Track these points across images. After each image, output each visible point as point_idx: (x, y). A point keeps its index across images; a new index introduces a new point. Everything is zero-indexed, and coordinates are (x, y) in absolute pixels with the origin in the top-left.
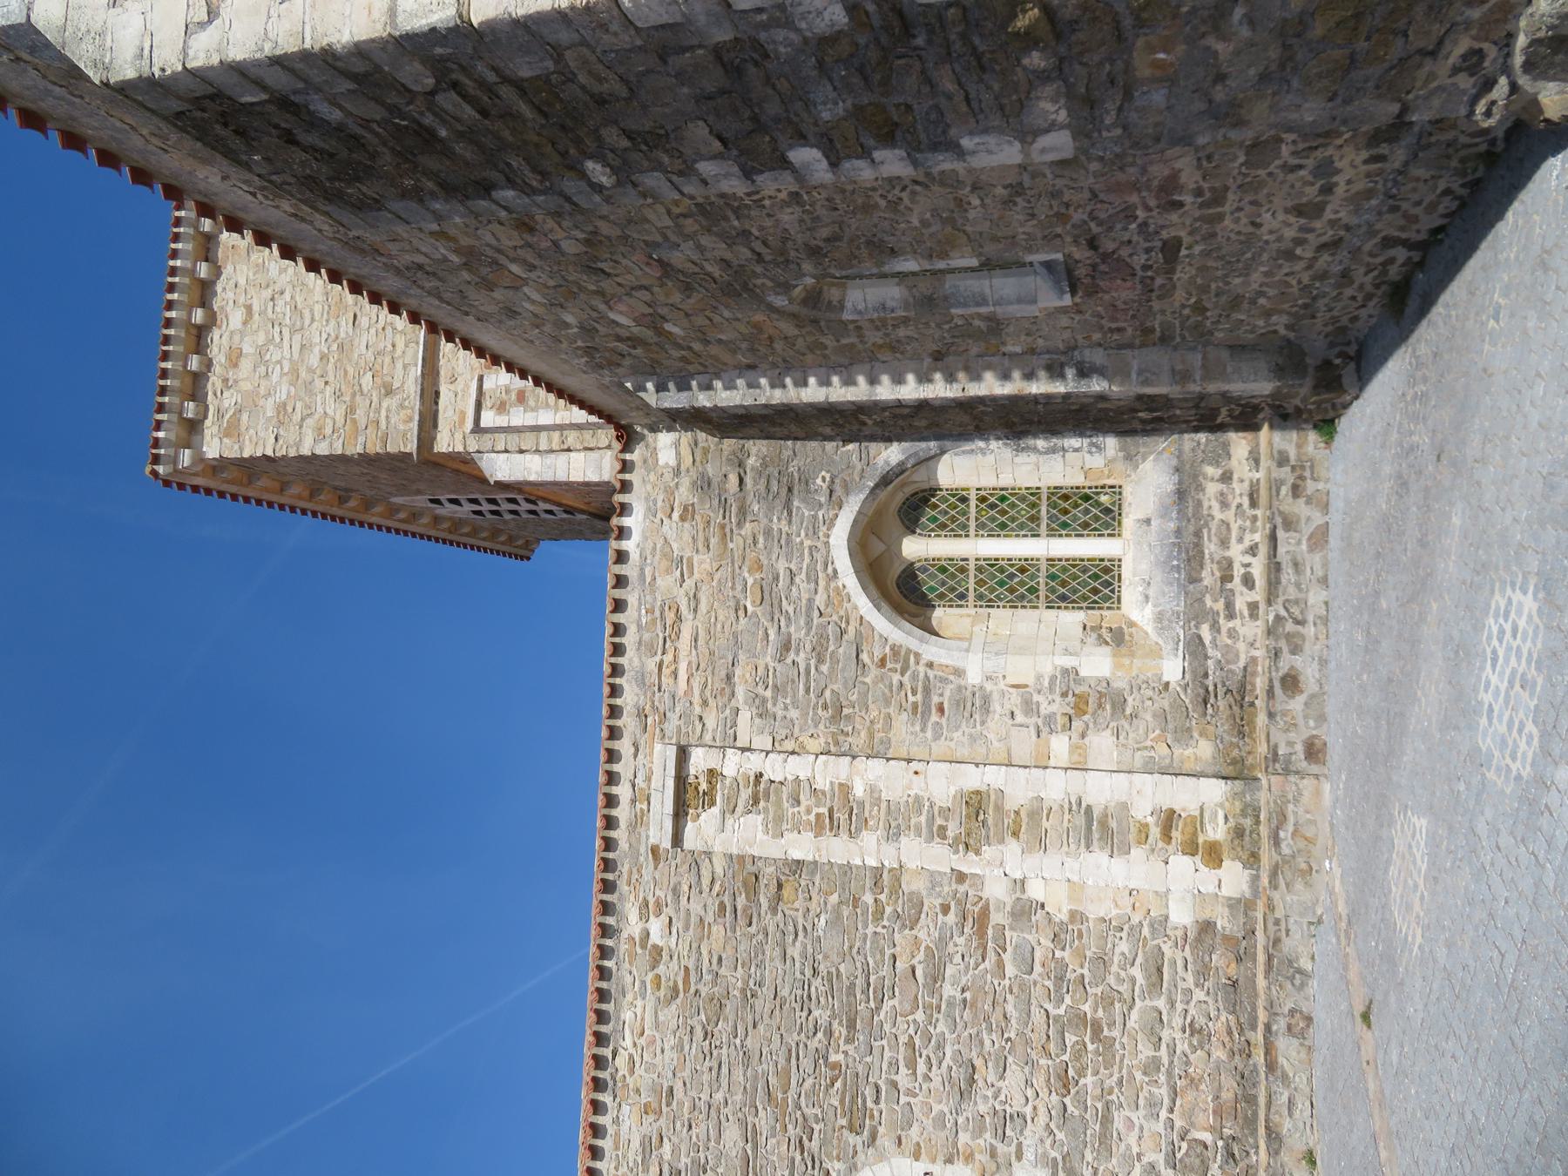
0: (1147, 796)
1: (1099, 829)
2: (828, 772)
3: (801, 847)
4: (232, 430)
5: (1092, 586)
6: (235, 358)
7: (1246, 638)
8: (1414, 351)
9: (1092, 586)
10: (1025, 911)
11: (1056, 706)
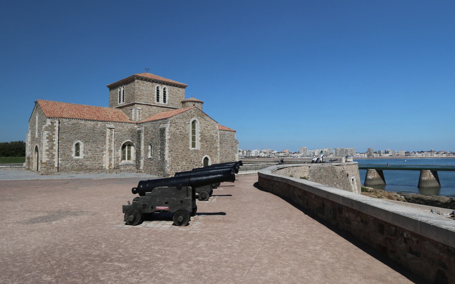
0: (113, 163)
1: (110, 160)
2: (113, 140)
3: (107, 138)
4: (138, 82)
5: (124, 158)
6: (144, 83)
7: (122, 169)
8: (400, 277)
9: (124, 158)
10: (103, 154)
11: (117, 156)
